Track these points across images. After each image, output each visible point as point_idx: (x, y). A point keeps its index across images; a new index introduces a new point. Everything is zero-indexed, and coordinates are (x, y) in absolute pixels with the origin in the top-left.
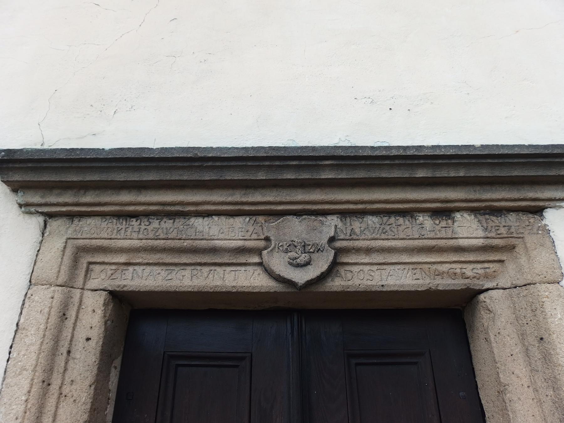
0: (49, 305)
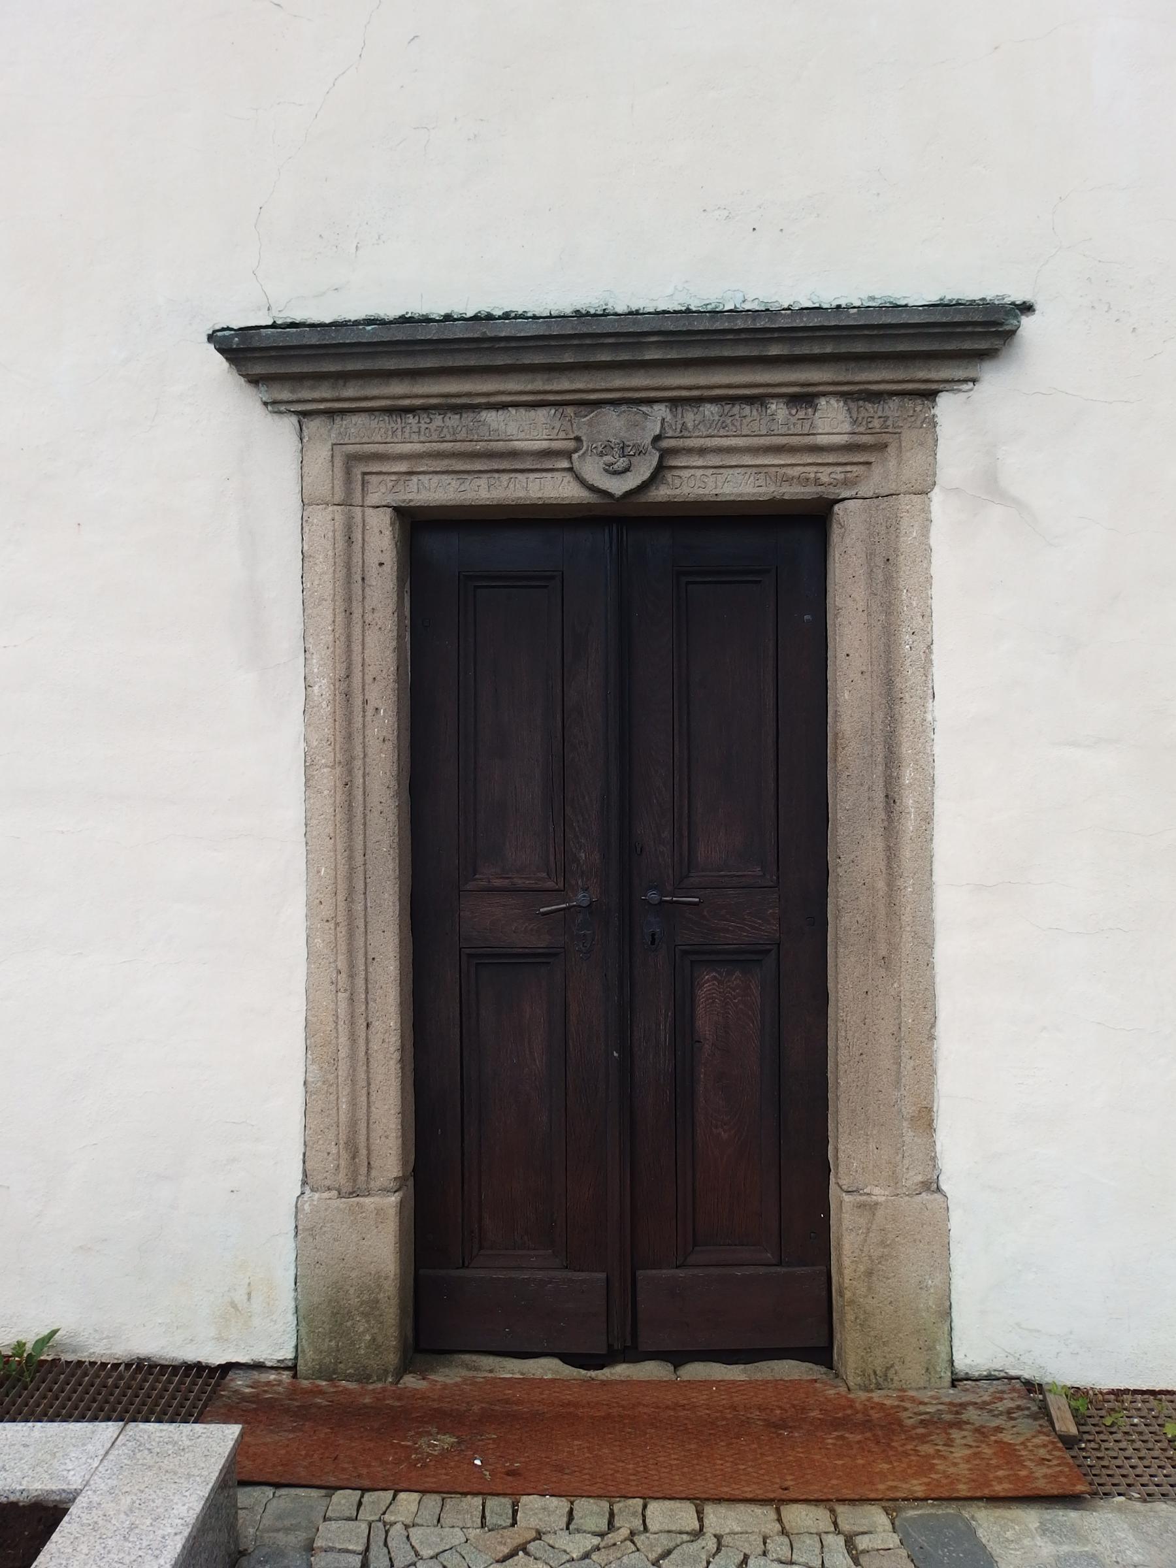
0: (332, 529)
